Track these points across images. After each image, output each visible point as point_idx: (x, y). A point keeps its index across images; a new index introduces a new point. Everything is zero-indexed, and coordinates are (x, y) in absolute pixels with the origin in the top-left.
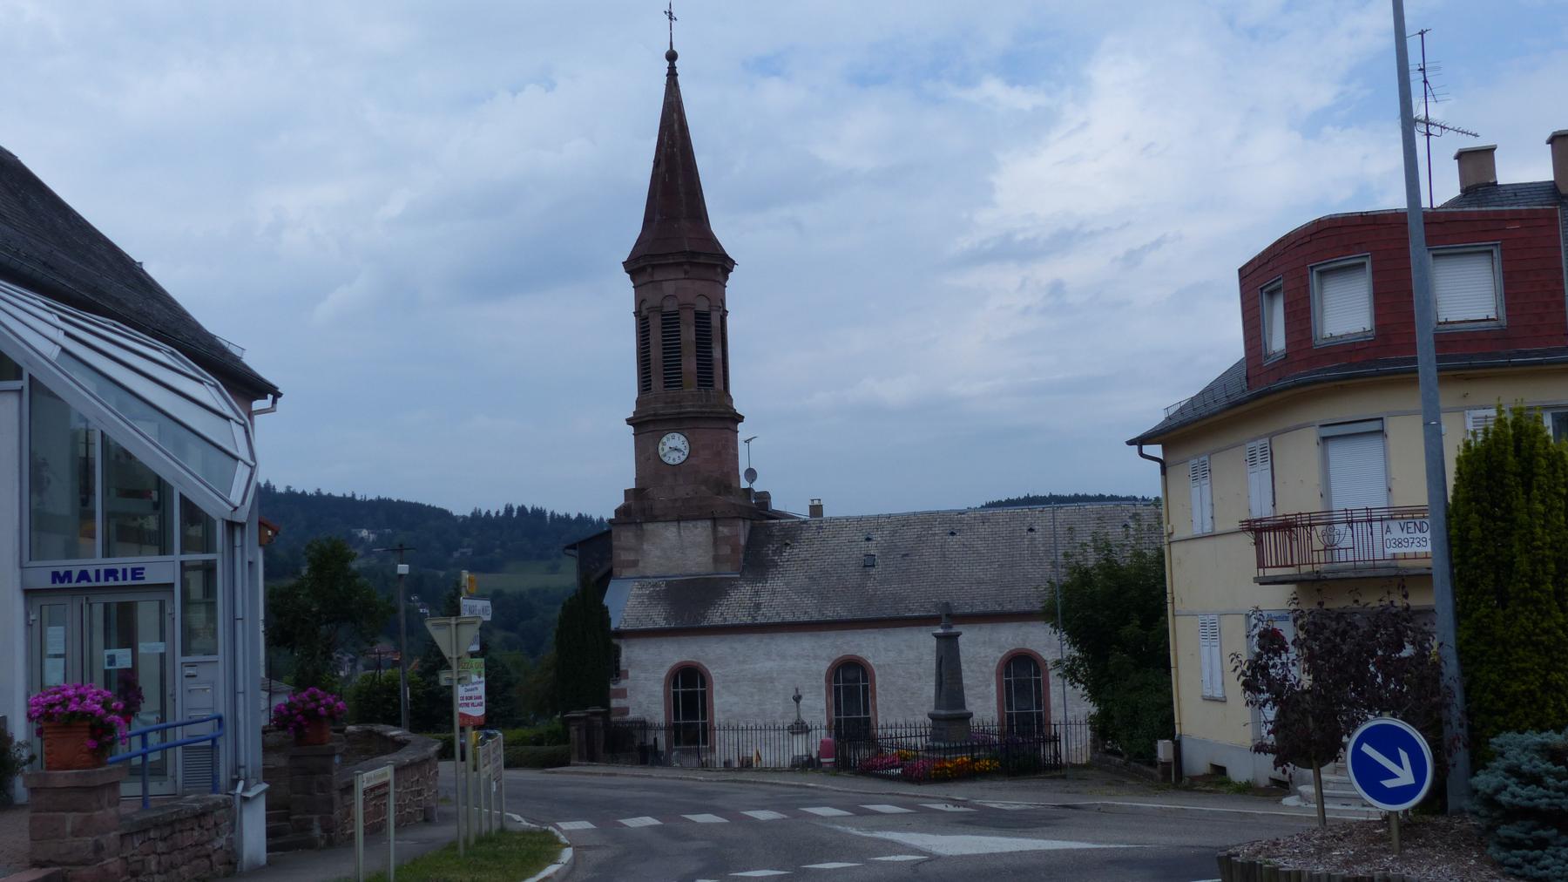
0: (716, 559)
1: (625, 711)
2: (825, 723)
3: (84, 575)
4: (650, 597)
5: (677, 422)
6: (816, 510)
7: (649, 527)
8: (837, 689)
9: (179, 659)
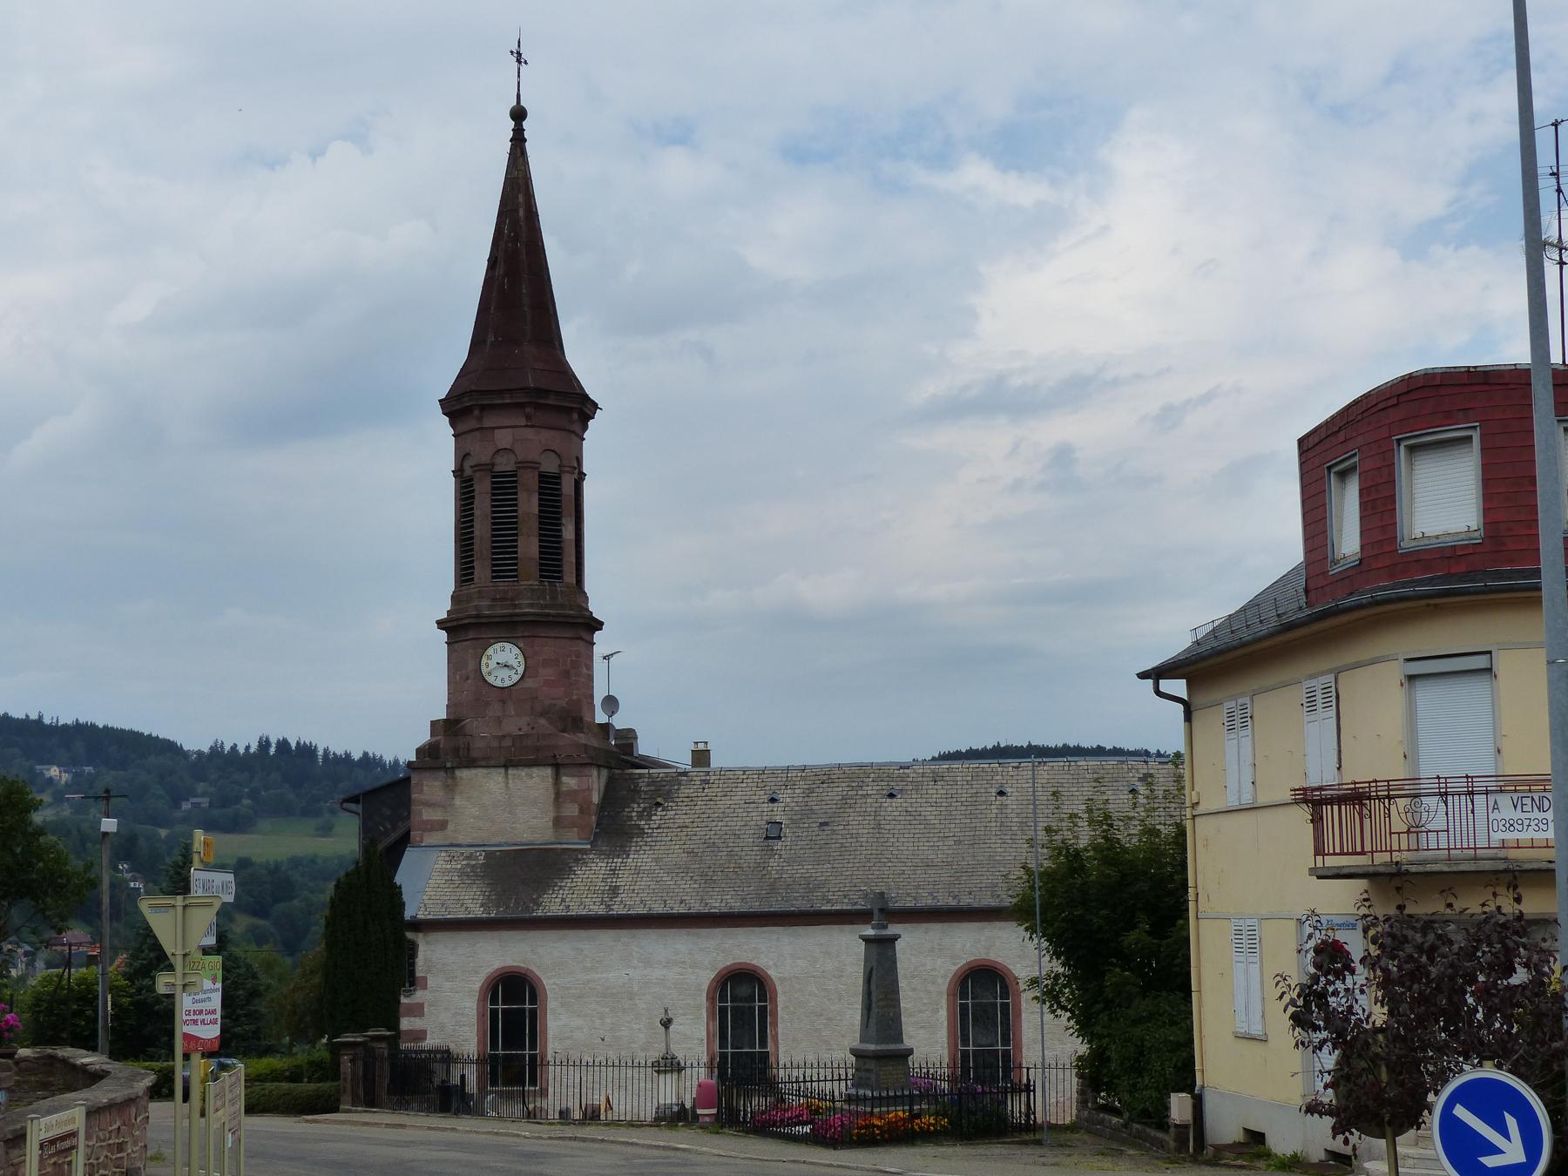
0: (558, 822)
1: (420, 1035)
2: (705, 1059)
5: (508, 627)
6: (701, 757)
7: (464, 774)
8: (723, 1011)
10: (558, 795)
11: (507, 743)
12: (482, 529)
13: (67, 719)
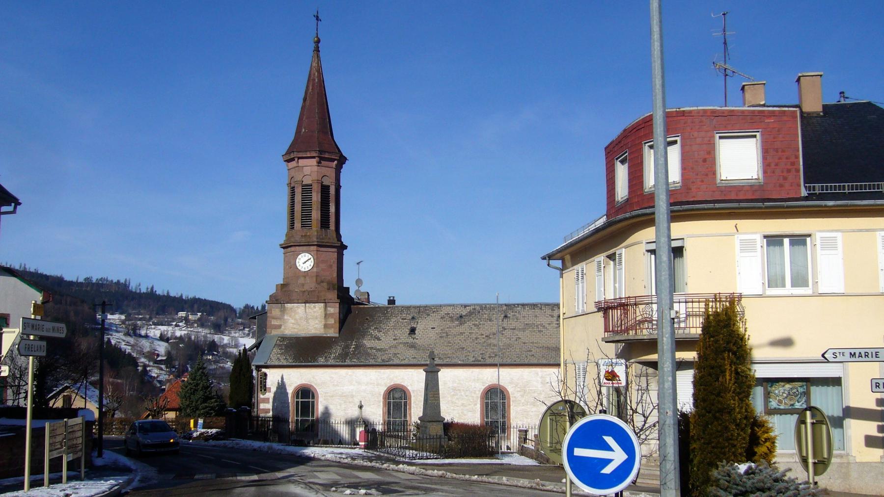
2: (381, 422)
4: (286, 346)
5: (305, 245)
6: (392, 302)
7: (289, 306)
8: (389, 403)
10: (326, 315)
12: (298, 208)
13: (191, 296)
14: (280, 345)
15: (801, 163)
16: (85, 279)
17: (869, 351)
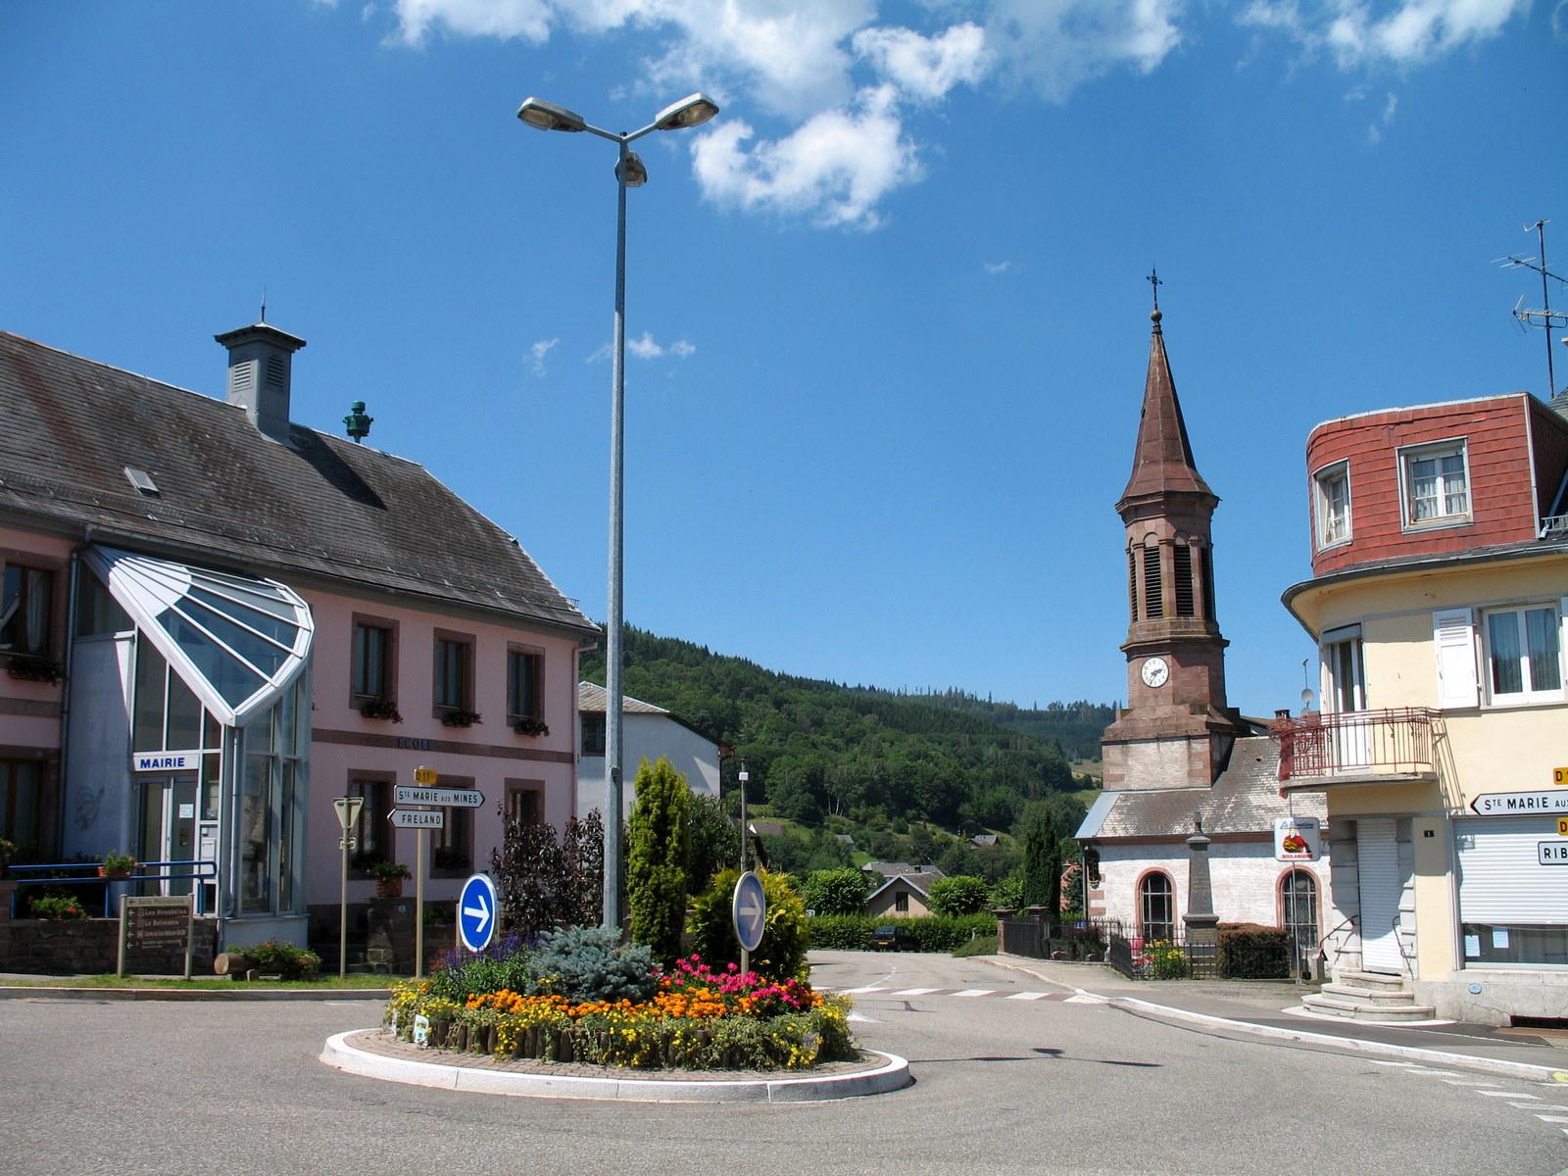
0: (1190, 774)
1: (1102, 911)
3: (156, 763)
4: (1130, 809)
9: (198, 822)
11: (1159, 723)
14: (1120, 807)
15: (1533, 484)
16: (1050, 707)
17: (1534, 796)
